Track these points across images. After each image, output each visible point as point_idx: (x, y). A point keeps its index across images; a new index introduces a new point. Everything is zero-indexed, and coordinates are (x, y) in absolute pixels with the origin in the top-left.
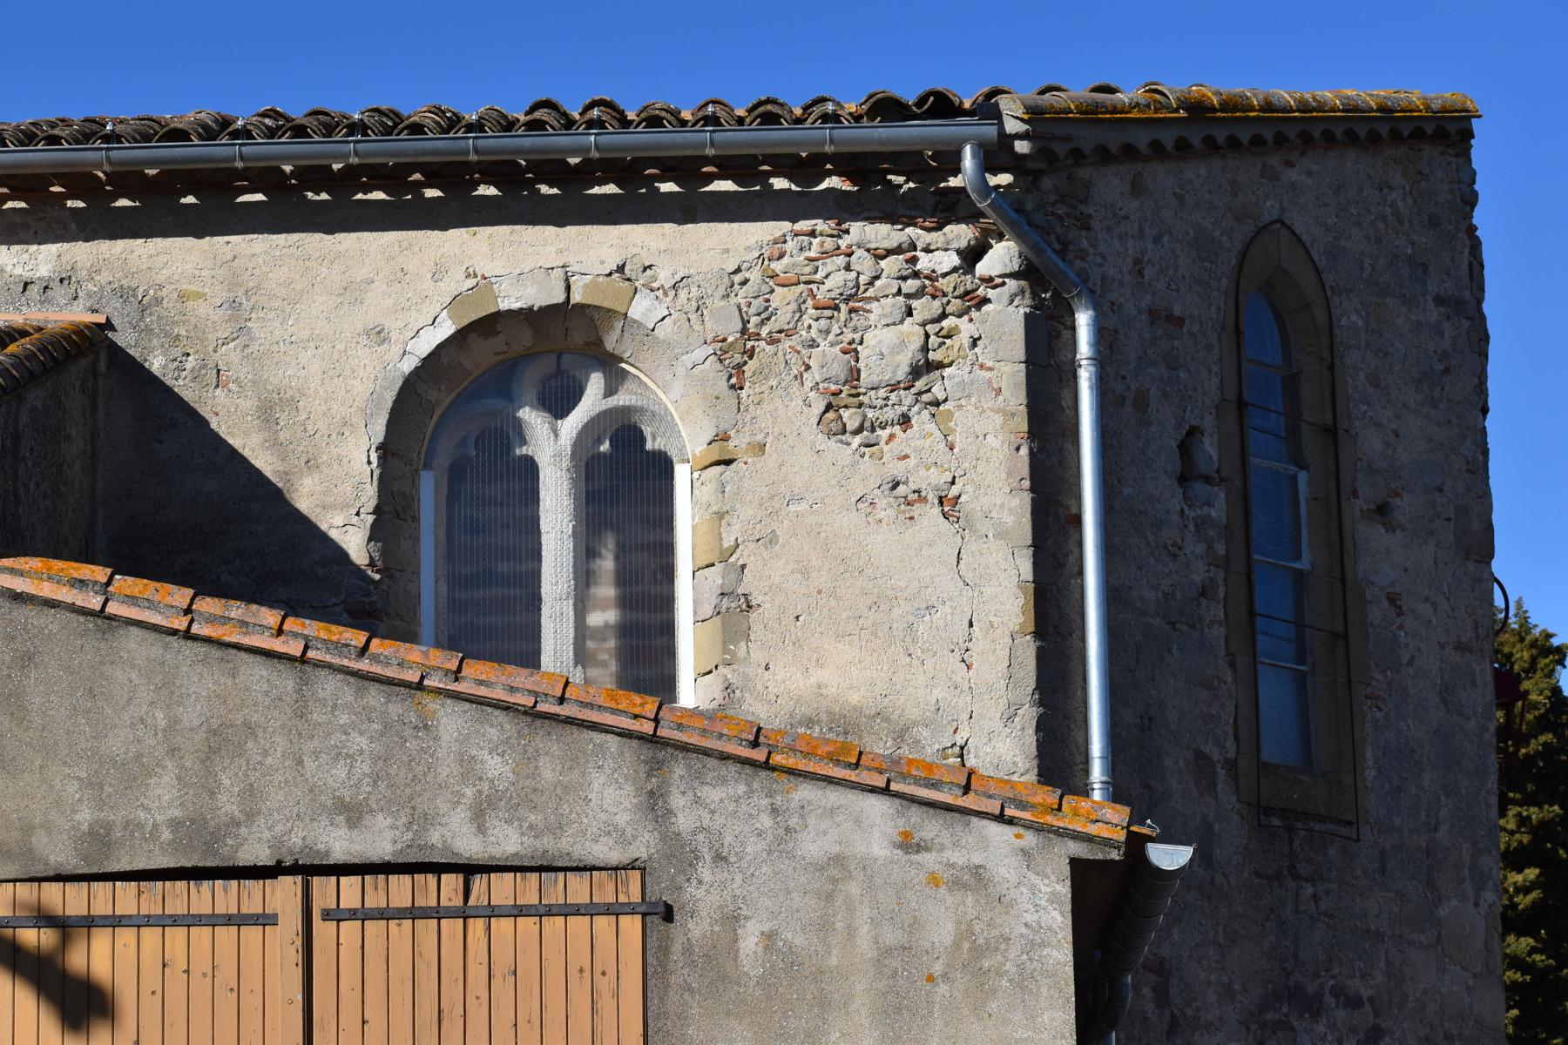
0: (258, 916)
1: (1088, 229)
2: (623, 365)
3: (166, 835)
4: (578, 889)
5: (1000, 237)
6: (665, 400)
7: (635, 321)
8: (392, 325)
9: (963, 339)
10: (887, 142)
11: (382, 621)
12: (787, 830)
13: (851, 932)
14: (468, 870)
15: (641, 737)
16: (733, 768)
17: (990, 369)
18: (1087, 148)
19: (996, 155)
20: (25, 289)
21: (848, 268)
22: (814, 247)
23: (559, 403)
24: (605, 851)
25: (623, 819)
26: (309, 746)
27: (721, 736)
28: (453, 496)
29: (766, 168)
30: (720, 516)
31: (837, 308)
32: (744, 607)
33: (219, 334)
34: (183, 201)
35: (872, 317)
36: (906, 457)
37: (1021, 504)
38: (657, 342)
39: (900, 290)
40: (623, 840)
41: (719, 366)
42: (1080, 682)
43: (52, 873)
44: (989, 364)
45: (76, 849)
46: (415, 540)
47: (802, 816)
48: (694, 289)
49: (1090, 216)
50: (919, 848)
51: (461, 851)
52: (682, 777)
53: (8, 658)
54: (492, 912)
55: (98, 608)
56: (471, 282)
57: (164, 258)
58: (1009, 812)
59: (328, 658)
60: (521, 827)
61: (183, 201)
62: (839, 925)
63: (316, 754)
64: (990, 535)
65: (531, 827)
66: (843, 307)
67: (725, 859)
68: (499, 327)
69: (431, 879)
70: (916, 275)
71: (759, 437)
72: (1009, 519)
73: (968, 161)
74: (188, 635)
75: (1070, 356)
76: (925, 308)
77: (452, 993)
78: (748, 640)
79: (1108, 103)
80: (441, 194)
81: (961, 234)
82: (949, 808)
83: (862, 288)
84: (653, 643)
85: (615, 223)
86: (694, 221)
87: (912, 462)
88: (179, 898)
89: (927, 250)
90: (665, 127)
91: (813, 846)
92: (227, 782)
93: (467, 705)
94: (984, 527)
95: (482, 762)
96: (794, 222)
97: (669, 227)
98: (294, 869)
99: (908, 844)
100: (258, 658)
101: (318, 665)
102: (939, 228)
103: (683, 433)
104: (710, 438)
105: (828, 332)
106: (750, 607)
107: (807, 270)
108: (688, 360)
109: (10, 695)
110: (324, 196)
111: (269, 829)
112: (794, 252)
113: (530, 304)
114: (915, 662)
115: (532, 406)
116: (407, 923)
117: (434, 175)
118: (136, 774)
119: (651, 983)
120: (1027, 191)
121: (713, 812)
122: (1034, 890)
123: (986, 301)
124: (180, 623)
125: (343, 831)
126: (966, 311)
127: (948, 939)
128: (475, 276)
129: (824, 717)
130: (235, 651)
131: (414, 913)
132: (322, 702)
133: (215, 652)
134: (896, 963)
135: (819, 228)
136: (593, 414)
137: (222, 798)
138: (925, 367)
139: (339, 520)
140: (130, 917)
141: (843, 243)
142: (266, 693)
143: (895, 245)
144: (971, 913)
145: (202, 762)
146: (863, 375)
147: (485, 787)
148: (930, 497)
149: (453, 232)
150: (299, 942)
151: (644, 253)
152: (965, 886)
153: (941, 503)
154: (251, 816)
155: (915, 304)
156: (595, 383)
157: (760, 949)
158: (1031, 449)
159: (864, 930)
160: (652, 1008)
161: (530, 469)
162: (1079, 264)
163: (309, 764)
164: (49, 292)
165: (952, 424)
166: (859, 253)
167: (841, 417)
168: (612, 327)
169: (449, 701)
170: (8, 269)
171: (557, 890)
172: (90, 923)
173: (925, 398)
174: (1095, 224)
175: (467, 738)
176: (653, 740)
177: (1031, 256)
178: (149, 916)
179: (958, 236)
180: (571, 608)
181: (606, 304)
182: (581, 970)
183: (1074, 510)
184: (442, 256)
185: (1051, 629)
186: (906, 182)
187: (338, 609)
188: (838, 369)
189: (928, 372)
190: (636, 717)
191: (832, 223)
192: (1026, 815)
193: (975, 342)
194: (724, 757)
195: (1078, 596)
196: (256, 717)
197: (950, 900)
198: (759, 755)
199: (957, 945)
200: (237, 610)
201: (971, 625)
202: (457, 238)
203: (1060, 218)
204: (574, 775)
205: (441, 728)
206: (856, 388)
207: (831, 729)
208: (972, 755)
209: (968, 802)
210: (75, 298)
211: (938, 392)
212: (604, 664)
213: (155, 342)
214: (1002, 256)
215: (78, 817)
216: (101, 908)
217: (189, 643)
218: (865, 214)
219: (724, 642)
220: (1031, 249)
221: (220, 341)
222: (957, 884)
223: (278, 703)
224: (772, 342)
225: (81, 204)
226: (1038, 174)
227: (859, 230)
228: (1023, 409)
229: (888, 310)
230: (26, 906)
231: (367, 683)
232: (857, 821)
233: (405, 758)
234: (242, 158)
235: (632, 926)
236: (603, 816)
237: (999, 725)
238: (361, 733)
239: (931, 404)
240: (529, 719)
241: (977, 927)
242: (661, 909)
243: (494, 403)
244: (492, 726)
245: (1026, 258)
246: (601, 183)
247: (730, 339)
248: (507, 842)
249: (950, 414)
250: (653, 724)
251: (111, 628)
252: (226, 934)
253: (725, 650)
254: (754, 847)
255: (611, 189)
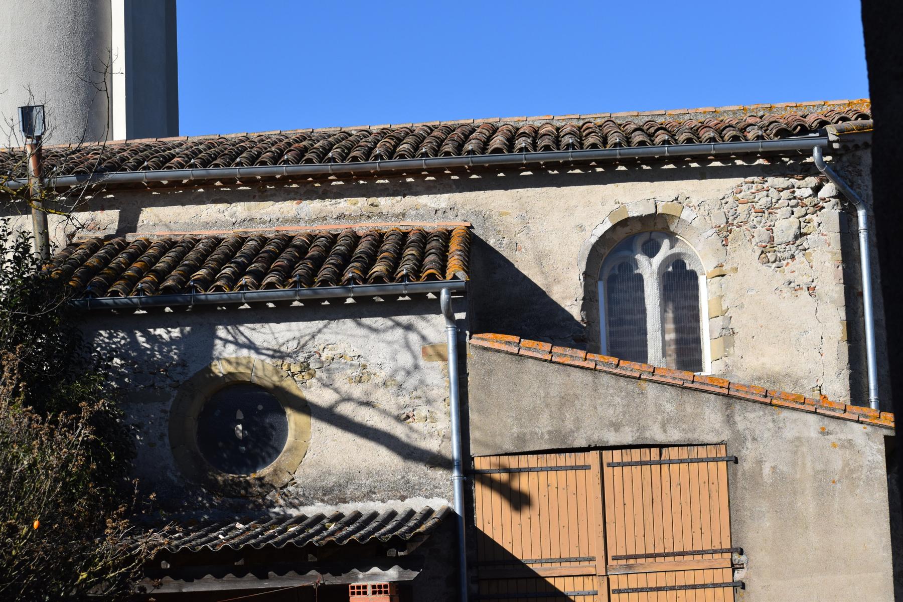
0: (583, 466)
1: (861, 176)
2: (677, 236)
3: (546, 437)
4: (702, 452)
5: (828, 181)
6: (696, 251)
7: (683, 220)
8: (586, 224)
9: (815, 223)
10: (784, 146)
11: (587, 342)
12: (779, 428)
13: (804, 465)
14: (661, 446)
15: (723, 395)
16: (758, 405)
17: (826, 235)
18: (860, 144)
19: (825, 151)
20: (436, 213)
21: (767, 196)
22: (753, 188)
23: (651, 251)
24: (712, 438)
25: (717, 426)
26: (599, 401)
27: (753, 394)
28: (610, 291)
29: (733, 156)
30: (721, 297)
31: (764, 212)
32: (732, 333)
33: (516, 229)
34: (499, 175)
35: (778, 215)
36: (794, 272)
37: (841, 288)
38: (692, 227)
39: (788, 204)
40: (718, 433)
41: (718, 237)
42: (864, 359)
43: (504, 453)
44: (825, 233)
45: (512, 443)
46: (598, 310)
47: (784, 423)
48: (707, 206)
49: (861, 170)
50: (828, 433)
51: (657, 439)
52: (739, 409)
53: (483, 372)
54: (670, 462)
55: (517, 352)
56: (617, 206)
57: (492, 199)
58: (861, 419)
59: (605, 369)
60: (680, 430)
61: (499, 175)
62: (799, 463)
63: (602, 405)
64: (828, 302)
65: (683, 430)
66: (766, 211)
67: (756, 440)
68: (628, 223)
69: (647, 450)
70: (795, 198)
71: (735, 265)
72: (836, 296)
73: (816, 151)
74: (551, 362)
75: (856, 228)
76: (799, 211)
77: (657, 492)
78: (734, 346)
79: (868, 124)
80: (603, 170)
81: (812, 181)
82: (839, 418)
83: (774, 204)
84: (636, 327)
85: (674, 180)
86: (705, 178)
87: (796, 273)
88: (553, 460)
89: (799, 188)
90: (695, 143)
91: (789, 433)
92: (568, 416)
93: (657, 385)
94: (826, 299)
95: (664, 406)
96: (745, 177)
97: (695, 181)
98: (595, 448)
99: (824, 432)
100: (578, 369)
101: (601, 371)
102: (803, 179)
103: (702, 263)
104: (715, 266)
105: (761, 222)
106: (734, 333)
107: (752, 197)
108: (705, 235)
109: (484, 386)
110: (556, 172)
111: (586, 433)
112: (746, 190)
113: (641, 214)
114: (800, 353)
115: (641, 254)
116: (639, 467)
117: (600, 163)
118: (534, 414)
119: (730, 487)
120: (837, 162)
121: (751, 422)
122: (871, 448)
123: (823, 208)
124: (548, 357)
125: (613, 433)
126: (815, 212)
127: (840, 468)
128: (619, 203)
129: (765, 376)
130: (569, 367)
131: (641, 463)
132: (603, 385)
133: (561, 368)
134: (821, 476)
135: (755, 180)
136: (666, 256)
137: (567, 422)
138: (800, 235)
139: (569, 303)
140: (534, 468)
141: (765, 186)
142: (582, 383)
143: (786, 186)
144: (848, 457)
145: (559, 409)
146: (775, 239)
147: (666, 415)
148: (804, 287)
149: (608, 185)
150: (599, 476)
151: (686, 192)
152: (846, 447)
153: (808, 290)
154: (578, 429)
155: (795, 210)
156: (666, 243)
157: (771, 473)
158: (843, 267)
159: (809, 464)
160: (731, 496)
161: (640, 278)
162: (858, 190)
163: (599, 409)
164: (446, 214)
165: (811, 258)
166: (772, 190)
167: (767, 256)
168: (673, 222)
169: (650, 383)
170: (429, 204)
171: (695, 453)
172: (519, 471)
173: (800, 247)
174: (863, 174)
175: (658, 397)
176: (728, 396)
177: (840, 189)
178: (541, 468)
179: (811, 182)
180: (660, 335)
181: (672, 213)
182: (705, 483)
183: (860, 290)
184: (605, 195)
185: (853, 339)
186: (789, 160)
187: (570, 339)
188: (765, 236)
189: (801, 237)
190: (721, 387)
191: (761, 178)
192: (867, 420)
193: (819, 225)
194: (755, 402)
195: (862, 325)
196: (578, 391)
197: (840, 452)
198: (768, 400)
199: (843, 469)
200: (569, 351)
201: (822, 338)
202: (610, 187)
203: (850, 172)
204: (699, 410)
205: (648, 393)
206: (773, 244)
207: (768, 381)
208: (824, 390)
209: (846, 416)
210: (457, 216)
211: (805, 245)
212: (670, 356)
213: (490, 233)
214: (829, 189)
215: (513, 431)
216: (523, 465)
217: (552, 364)
218: (773, 174)
219: (724, 348)
220: (841, 187)
221: (517, 232)
222: (843, 446)
223: (586, 386)
224: (739, 227)
225: (457, 178)
226: (841, 155)
227: (772, 181)
228: (839, 251)
229: (784, 213)
230: (495, 465)
231: (619, 377)
232: (805, 424)
233: (635, 405)
234: (526, 159)
235: (723, 465)
236: (710, 425)
237: (834, 378)
238: (618, 396)
239: (803, 250)
240: (681, 389)
241: (850, 463)
242: (734, 459)
243: (626, 253)
244: (667, 392)
245: (838, 190)
246: (668, 164)
247: (722, 226)
248: (674, 435)
249: (810, 254)
250: (727, 390)
251: (521, 359)
252: (571, 473)
253: (725, 351)
254: (767, 435)
255: (671, 166)
